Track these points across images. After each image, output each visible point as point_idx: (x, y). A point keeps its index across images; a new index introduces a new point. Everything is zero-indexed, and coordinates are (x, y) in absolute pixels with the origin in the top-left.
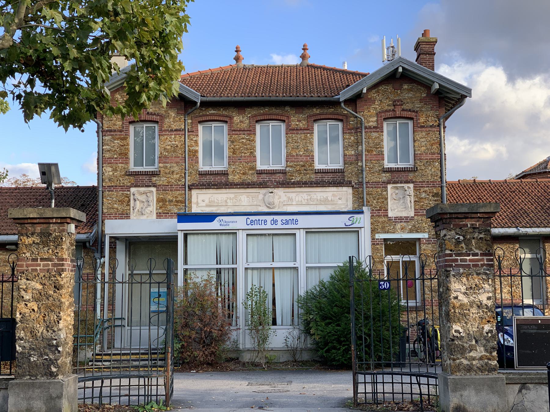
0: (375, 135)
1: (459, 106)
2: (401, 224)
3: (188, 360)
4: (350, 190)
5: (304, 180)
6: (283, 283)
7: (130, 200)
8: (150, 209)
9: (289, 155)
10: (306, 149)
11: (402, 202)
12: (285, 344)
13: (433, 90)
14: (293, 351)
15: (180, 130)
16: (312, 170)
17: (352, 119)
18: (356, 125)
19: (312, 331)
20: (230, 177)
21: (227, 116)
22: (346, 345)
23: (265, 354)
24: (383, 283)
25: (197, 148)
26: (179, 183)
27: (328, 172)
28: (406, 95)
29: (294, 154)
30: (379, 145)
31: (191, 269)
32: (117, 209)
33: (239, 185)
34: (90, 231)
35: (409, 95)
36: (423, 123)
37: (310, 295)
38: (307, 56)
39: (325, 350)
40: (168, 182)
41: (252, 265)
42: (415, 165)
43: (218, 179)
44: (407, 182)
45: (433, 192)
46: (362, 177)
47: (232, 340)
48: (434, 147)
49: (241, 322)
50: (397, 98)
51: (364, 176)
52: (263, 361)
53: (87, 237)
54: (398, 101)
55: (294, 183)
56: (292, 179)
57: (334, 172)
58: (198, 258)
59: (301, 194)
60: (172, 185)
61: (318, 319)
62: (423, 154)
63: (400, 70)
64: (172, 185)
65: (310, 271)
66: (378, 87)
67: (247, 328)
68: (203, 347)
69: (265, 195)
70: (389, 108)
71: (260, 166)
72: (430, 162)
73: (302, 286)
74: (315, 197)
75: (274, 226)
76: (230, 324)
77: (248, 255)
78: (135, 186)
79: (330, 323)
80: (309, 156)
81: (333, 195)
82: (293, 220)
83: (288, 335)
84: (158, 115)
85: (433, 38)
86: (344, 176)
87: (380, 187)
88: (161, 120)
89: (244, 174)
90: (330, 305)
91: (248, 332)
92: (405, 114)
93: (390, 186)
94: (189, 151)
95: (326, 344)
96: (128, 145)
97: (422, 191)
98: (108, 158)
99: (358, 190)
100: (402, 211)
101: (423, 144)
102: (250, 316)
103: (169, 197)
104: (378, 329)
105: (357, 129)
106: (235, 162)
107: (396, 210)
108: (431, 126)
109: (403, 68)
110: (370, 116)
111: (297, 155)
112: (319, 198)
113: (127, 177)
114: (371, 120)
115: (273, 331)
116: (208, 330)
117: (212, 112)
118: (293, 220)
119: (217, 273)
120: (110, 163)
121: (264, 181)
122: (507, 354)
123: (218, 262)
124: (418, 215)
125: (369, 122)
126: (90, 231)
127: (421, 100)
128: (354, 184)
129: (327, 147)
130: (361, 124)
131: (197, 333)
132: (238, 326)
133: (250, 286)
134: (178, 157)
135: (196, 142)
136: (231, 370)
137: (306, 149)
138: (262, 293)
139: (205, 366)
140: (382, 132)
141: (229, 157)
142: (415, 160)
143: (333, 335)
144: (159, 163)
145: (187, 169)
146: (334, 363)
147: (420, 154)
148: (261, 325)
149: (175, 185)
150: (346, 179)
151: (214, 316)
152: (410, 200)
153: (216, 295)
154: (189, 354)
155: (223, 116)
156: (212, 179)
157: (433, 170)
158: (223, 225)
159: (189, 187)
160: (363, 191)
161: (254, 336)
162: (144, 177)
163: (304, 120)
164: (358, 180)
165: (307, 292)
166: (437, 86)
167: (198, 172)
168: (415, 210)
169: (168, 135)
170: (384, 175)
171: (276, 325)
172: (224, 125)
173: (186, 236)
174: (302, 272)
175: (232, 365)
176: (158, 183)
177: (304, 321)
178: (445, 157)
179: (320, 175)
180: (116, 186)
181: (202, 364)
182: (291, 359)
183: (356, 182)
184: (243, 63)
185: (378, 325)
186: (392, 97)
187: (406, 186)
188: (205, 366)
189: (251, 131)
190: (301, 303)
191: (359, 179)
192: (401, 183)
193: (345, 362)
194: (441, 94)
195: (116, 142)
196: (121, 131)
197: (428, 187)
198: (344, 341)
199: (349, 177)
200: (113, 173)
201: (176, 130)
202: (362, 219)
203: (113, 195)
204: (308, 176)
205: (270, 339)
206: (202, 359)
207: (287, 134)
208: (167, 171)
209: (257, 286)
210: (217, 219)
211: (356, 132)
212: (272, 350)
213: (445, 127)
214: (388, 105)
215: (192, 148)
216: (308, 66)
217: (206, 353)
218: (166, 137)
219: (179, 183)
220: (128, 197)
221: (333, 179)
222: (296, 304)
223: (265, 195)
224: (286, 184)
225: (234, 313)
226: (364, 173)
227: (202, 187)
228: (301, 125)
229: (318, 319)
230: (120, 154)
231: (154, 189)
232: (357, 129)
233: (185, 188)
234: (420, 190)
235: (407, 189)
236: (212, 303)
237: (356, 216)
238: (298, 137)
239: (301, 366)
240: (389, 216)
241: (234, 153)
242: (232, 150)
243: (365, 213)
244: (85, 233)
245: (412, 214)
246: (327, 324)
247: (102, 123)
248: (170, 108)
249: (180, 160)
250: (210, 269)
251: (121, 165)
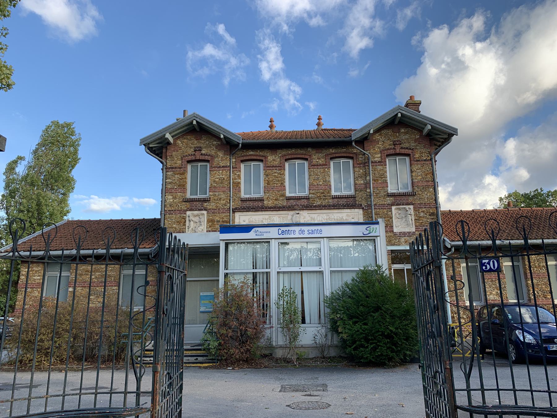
0: (379, 167)
2: (405, 238)
3: (225, 358)
4: (361, 211)
6: (310, 284)
7: (185, 221)
8: (202, 227)
9: (311, 185)
11: (404, 220)
12: (314, 342)
13: (425, 131)
14: (321, 348)
15: (226, 167)
17: (361, 156)
19: (340, 330)
20: (265, 202)
23: (296, 350)
24: (487, 261)
29: (316, 184)
33: (272, 208)
35: (406, 137)
38: (321, 124)
41: (283, 269)
43: (256, 204)
44: (408, 204)
46: (371, 201)
51: (373, 200)
52: (294, 358)
55: (315, 206)
58: (238, 262)
63: (399, 115)
69: (293, 216)
70: (391, 147)
71: (288, 194)
72: (425, 188)
73: (327, 288)
74: (333, 217)
75: (302, 236)
77: (280, 260)
78: (190, 210)
81: (347, 215)
84: (209, 155)
89: (276, 200)
91: (280, 329)
92: (403, 151)
93: (393, 208)
94: (233, 183)
95: (354, 342)
96: (186, 178)
99: (367, 209)
101: (419, 174)
102: (282, 315)
104: (405, 327)
105: (365, 164)
106: (269, 191)
108: (425, 160)
109: (402, 114)
112: (336, 218)
113: (184, 203)
114: (376, 156)
115: (302, 329)
116: (244, 328)
117: (252, 153)
119: (253, 276)
121: (292, 205)
122: (528, 351)
123: (255, 267)
124: (418, 231)
127: (416, 141)
129: (340, 178)
130: (368, 159)
131: (233, 331)
135: (239, 176)
136: (265, 367)
138: (292, 293)
143: (361, 334)
151: (249, 314)
152: (411, 218)
153: (252, 295)
156: (251, 204)
160: (372, 212)
165: (333, 293)
166: (429, 127)
168: (416, 226)
173: (227, 245)
174: (327, 275)
175: (265, 361)
176: (209, 207)
181: (238, 360)
184: (274, 130)
186: (392, 138)
187: (407, 207)
188: (241, 362)
189: (282, 167)
190: (327, 303)
191: (368, 203)
192: (403, 205)
193: (373, 360)
194: (431, 136)
196: (180, 168)
198: (372, 339)
201: (223, 167)
206: (237, 357)
207: (309, 169)
208: (216, 198)
209: (288, 287)
211: (364, 166)
212: (302, 347)
213: (435, 161)
214: (390, 145)
217: (242, 350)
218: (215, 172)
221: (348, 203)
223: (293, 216)
224: (310, 207)
226: (372, 197)
231: (205, 212)
232: (365, 164)
236: (247, 303)
237: (372, 226)
238: (319, 171)
241: (268, 184)
245: (413, 230)
246: (355, 323)
250: (247, 273)
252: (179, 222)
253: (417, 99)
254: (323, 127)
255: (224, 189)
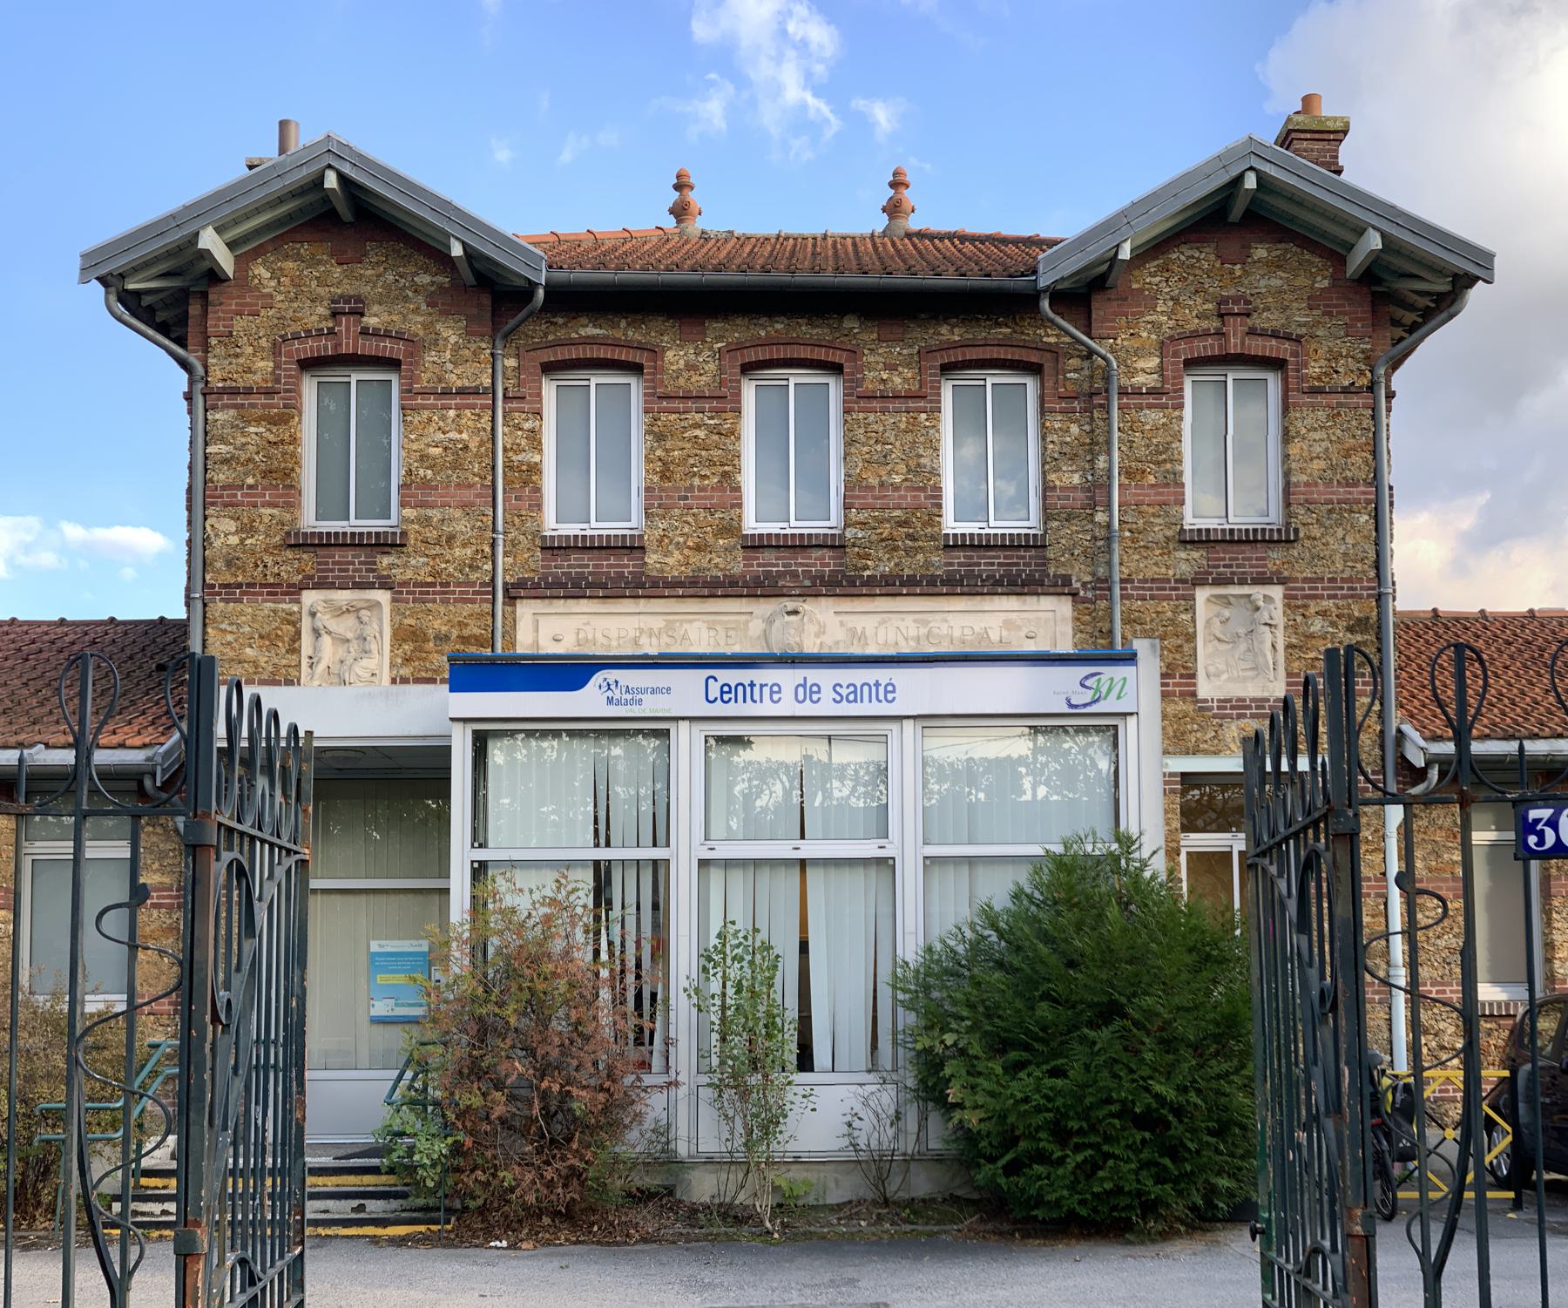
0: (1153, 417)
1: (1444, 316)
2: (1242, 722)
3: (480, 1202)
5: (907, 572)
7: (298, 633)
8: (370, 663)
10: (912, 464)
11: (1243, 647)
12: (846, 1142)
13: (1356, 261)
14: (877, 1166)
15: (475, 392)
16: (933, 538)
17: (1074, 362)
18: (1086, 386)
19: (954, 1094)
20: (652, 559)
21: (640, 348)
22: (1090, 1146)
23: (771, 1175)
24: (1545, 813)
25: (537, 458)
26: (474, 576)
27: (988, 547)
28: (1263, 283)
29: (874, 481)
30: (1165, 455)
31: (499, 863)
32: (255, 664)
33: (680, 584)
34: (162, 739)
35: (1273, 284)
36: (1319, 379)
37: (939, 962)
39: (1001, 1163)
40: (435, 574)
42: (1288, 524)
43: (608, 565)
45: (1350, 617)
46: (1109, 564)
47: (648, 1124)
48: (1354, 459)
49: (684, 1057)
50: (1232, 292)
51: (1116, 560)
53: (148, 759)
54: (1236, 300)
56: (866, 568)
57: (1011, 547)
59: (895, 620)
60: (448, 584)
61: (975, 1050)
62: (1316, 485)
63: (1251, 182)
64: (448, 584)
65: (936, 872)
66: (1167, 252)
67: (705, 1079)
68: (539, 1151)
69: (770, 621)
71: (752, 524)
72: (1340, 511)
76: (645, 1065)
77: (709, 813)
78: (319, 586)
79: (1019, 1066)
80: (923, 489)
82: (877, 684)
83: (858, 1108)
84: (399, 337)
85: (1335, 119)
86: (1045, 562)
87: (1169, 598)
88: (411, 354)
89: (698, 548)
90: (1018, 994)
91: (707, 1094)
92: (1257, 346)
93: (1202, 595)
94: (508, 466)
95: (1010, 1141)
96: (294, 440)
97: (1312, 610)
98: (223, 488)
99: (1092, 601)
100: (1245, 679)
101: (1318, 449)
102: (715, 1036)
103: (438, 625)
105: (1092, 398)
106: (668, 508)
107: (1225, 676)
108: (1346, 391)
110: (1138, 353)
111: (882, 484)
112: (957, 633)
113: (289, 554)
114: (1141, 364)
115: (800, 1090)
116: (556, 1088)
118: (877, 684)
120: (232, 505)
123: (602, 836)
125: (1133, 373)
126: (162, 739)
127: (1313, 301)
128: (1078, 585)
129: (983, 461)
130: (1107, 379)
132: (672, 1072)
133: (715, 926)
134: (470, 486)
136: (644, 1240)
137: (912, 464)
139: (546, 1220)
140: (1181, 406)
141: (647, 489)
142: (1288, 505)
143: (1039, 1109)
144: (403, 505)
145: (500, 528)
146: (1039, 1213)
147: (1307, 484)
148: (755, 1069)
149: (459, 584)
150: (1051, 571)
152: (1273, 641)
153: (590, 956)
154: (483, 1178)
155: (628, 346)
156: (588, 565)
157: (1349, 540)
158: (619, 703)
159: (506, 590)
161: (731, 1113)
162: (350, 554)
163: (908, 366)
164: (1093, 575)
165: (929, 949)
166: (1374, 242)
167: (538, 542)
169: (434, 407)
170: (1183, 555)
171: (811, 1070)
172: (632, 381)
174: (910, 875)
176: (398, 574)
177: (919, 1053)
178: (1391, 496)
179: (960, 557)
180: (249, 585)
181: (533, 1214)
182: (870, 1196)
183: (1088, 578)
184: (699, 224)
185: (1212, 1072)
187: (1258, 592)
188: (546, 1220)
189: (727, 403)
190: (904, 991)
192: (1242, 582)
193: (1084, 1212)
195: (252, 429)
196: (269, 393)
197: (1335, 597)
198: (1080, 1132)
199: (1064, 564)
200: (242, 541)
201: (462, 392)
202: (1131, 683)
203: (242, 613)
204: (920, 557)
205: (789, 1126)
207: (847, 411)
209: (743, 924)
210: (598, 678)
212: (797, 1161)
213: (1390, 396)
215: (520, 457)
216: (909, 235)
217: (549, 1174)
218: (426, 414)
219: (474, 576)
220: (293, 624)
221: (1008, 568)
222: (885, 993)
223: (770, 621)
225: (658, 1025)
226: (1116, 546)
227: (555, 592)
228: (897, 380)
229: (975, 1050)
230: (266, 474)
231: (383, 597)
232: (1092, 398)
233: (494, 593)
234: (1306, 606)
235: (1261, 603)
236: (572, 986)
237: (1108, 671)
238: (889, 422)
239: (907, 1221)
240: (1201, 694)
241: (664, 476)
242: (658, 466)
243: (1140, 663)
244: (145, 746)
247: (206, 367)
248: (442, 313)
249: (478, 496)
250: (570, 864)
251: (269, 511)
252: (270, 639)
253: (1329, 110)
254: (914, 223)
255: (469, 495)
